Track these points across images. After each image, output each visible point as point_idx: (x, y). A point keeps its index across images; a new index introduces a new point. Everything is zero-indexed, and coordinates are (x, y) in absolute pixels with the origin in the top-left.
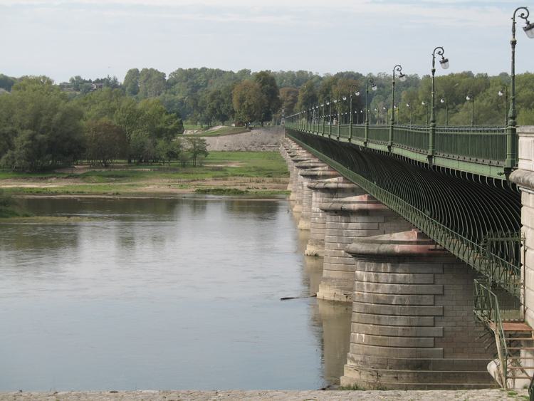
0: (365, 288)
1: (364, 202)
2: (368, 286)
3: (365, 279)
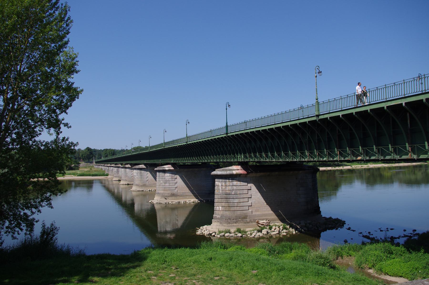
0: (221, 189)
1: (238, 170)
2: (222, 188)
3: (220, 185)
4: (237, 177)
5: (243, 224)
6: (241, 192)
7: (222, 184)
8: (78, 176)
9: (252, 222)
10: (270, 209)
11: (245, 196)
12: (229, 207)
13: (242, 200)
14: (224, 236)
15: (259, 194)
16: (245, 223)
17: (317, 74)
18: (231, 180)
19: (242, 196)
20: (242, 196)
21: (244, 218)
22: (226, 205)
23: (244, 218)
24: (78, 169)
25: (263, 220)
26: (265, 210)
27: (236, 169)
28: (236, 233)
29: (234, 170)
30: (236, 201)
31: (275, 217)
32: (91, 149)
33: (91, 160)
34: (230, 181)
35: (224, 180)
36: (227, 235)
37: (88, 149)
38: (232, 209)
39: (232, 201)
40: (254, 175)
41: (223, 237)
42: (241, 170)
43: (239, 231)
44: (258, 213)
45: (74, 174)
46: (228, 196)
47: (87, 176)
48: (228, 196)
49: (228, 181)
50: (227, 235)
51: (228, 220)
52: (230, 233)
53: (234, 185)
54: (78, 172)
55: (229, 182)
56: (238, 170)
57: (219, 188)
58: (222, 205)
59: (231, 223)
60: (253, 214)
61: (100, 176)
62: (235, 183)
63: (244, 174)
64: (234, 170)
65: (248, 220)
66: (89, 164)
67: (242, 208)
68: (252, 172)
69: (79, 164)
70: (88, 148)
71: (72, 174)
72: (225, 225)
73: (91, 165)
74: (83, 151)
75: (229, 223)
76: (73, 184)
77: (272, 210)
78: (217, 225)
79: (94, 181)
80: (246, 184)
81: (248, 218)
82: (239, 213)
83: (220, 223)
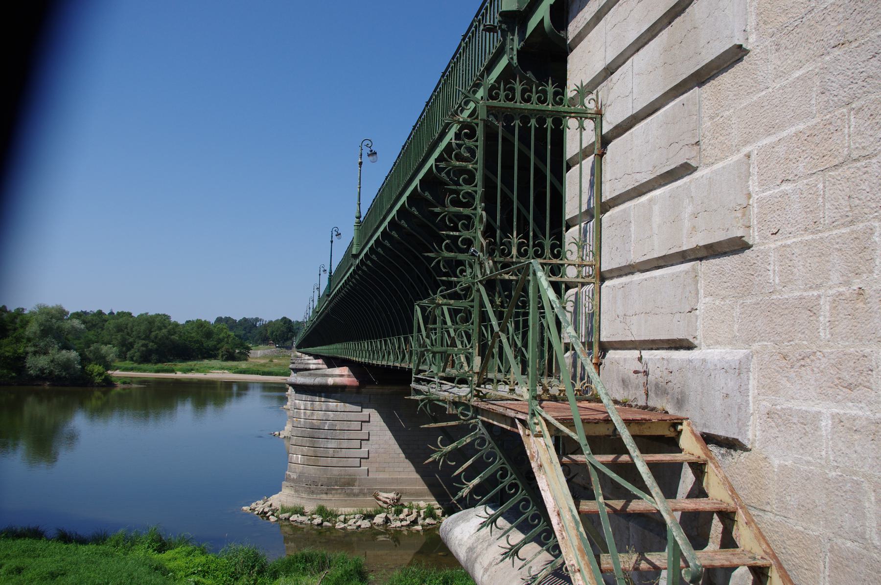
1: (342, 376)
3: (302, 407)
4: (336, 392)
5: (342, 497)
6: (345, 425)
7: (305, 405)
8: (235, 373)
9: (364, 495)
10: (413, 468)
11: (353, 435)
12: (314, 458)
13: (345, 444)
14: (287, 519)
15: (389, 433)
16: (348, 495)
17: (366, 159)
18: (325, 397)
19: (347, 435)
20: (347, 435)
21: (346, 485)
22: (311, 451)
23: (346, 485)
24: (246, 360)
25: (386, 491)
26: (401, 469)
27: (341, 376)
28: (314, 516)
29: (332, 376)
30: (333, 444)
31: (422, 487)
32: (290, 321)
33: (288, 343)
34: (323, 399)
35: (309, 398)
36: (294, 518)
37: (285, 321)
38: (323, 462)
39: (322, 443)
40: (376, 389)
41: (286, 523)
42: (349, 376)
43: (321, 511)
44: (381, 476)
45: (229, 369)
46: (317, 433)
47: (252, 374)
48: (317, 433)
49: (317, 399)
50: (294, 518)
51: (312, 486)
52: (303, 514)
53: (331, 408)
54: (243, 365)
55: (319, 403)
56: (342, 376)
57: (300, 414)
58: (302, 451)
59: (317, 494)
60: (371, 476)
61: (277, 375)
62: (333, 404)
63: (351, 387)
64: (332, 376)
65: (356, 489)
66: (284, 350)
67: (344, 462)
68: (371, 383)
69: (249, 349)
70: (284, 318)
71: (227, 369)
72: (304, 495)
73: (288, 352)
74: (176, 325)
75: (313, 492)
76: (235, 388)
77: (417, 472)
78: (288, 495)
79: (251, 385)
80: (359, 408)
81: (357, 483)
82: (336, 471)
83: (296, 491)
